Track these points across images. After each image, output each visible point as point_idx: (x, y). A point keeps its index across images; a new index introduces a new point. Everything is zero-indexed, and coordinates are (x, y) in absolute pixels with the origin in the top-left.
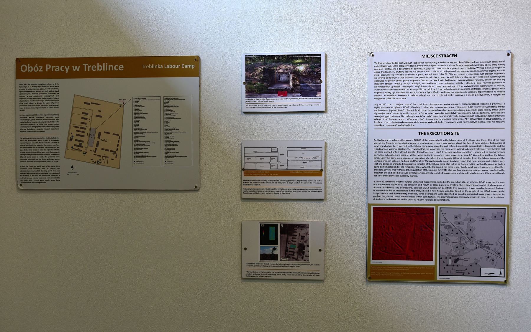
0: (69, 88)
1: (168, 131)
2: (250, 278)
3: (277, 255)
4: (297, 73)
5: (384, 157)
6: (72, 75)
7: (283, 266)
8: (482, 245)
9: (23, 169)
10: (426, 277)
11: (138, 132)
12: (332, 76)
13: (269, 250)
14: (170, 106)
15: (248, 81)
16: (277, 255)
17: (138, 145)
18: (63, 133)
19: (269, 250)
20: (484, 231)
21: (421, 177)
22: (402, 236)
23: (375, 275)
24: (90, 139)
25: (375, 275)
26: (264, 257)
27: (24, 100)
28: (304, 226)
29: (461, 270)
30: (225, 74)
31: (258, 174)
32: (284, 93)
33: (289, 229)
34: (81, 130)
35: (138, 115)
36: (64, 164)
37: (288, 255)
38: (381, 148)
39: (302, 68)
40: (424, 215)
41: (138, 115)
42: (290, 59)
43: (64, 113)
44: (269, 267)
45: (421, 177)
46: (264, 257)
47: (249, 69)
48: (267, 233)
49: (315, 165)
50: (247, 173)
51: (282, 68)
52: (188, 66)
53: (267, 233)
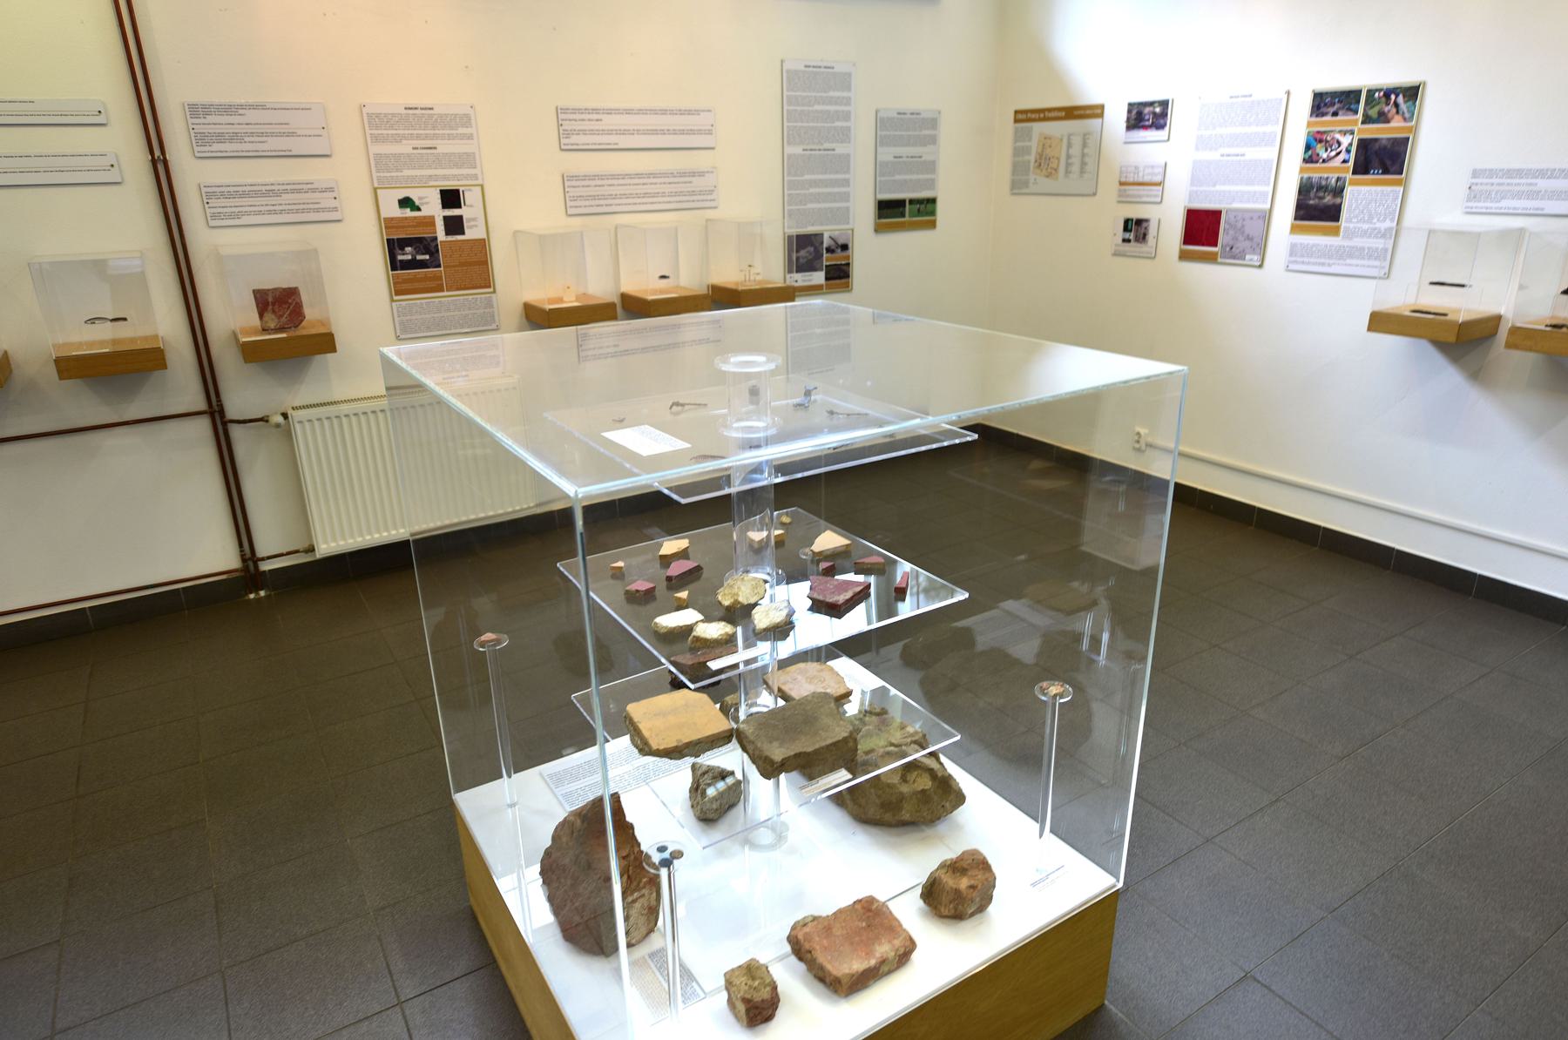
0: (1039, 128)
1: (1083, 155)
2: (1116, 254)
3: (463, 233)
4: (1154, 114)
5: (1199, 174)
6: (1040, 120)
7: (1133, 247)
8: (1249, 238)
9: (848, 172)
10: (1211, 259)
11: (1068, 157)
12: (1176, 117)
13: (1127, 235)
14: (1085, 137)
15: (1128, 119)
16: (463, 233)
17: (1068, 165)
18: (1032, 158)
19: (1127, 235)
20: (1253, 228)
21: (1218, 188)
22: (1202, 228)
23: (1184, 256)
24: (1045, 163)
25: (1184, 256)
26: (1124, 240)
27: (1018, 136)
28: (1147, 221)
29: (1234, 255)
30: (1116, 117)
31: (1129, 185)
32: (1145, 128)
33: (1139, 222)
34: (1041, 156)
35: (1069, 145)
36: (1032, 177)
37: (1137, 240)
38: (1197, 167)
39: (1158, 110)
40: (1215, 215)
41: (1069, 145)
42: (1151, 104)
43: (1034, 145)
44: (1127, 247)
45: (1218, 188)
46: (1124, 240)
47: (1129, 111)
48: (1128, 225)
49: (1158, 179)
50: (1122, 184)
51: (1147, 110)
52: (1096, 112)
53: (1128, 225)
